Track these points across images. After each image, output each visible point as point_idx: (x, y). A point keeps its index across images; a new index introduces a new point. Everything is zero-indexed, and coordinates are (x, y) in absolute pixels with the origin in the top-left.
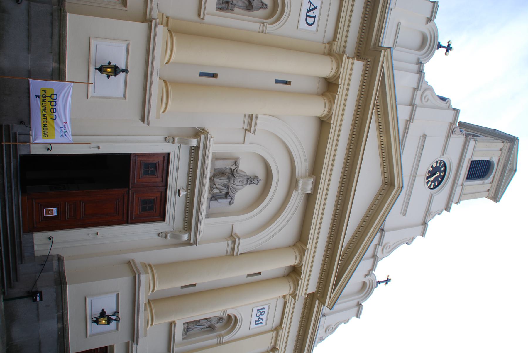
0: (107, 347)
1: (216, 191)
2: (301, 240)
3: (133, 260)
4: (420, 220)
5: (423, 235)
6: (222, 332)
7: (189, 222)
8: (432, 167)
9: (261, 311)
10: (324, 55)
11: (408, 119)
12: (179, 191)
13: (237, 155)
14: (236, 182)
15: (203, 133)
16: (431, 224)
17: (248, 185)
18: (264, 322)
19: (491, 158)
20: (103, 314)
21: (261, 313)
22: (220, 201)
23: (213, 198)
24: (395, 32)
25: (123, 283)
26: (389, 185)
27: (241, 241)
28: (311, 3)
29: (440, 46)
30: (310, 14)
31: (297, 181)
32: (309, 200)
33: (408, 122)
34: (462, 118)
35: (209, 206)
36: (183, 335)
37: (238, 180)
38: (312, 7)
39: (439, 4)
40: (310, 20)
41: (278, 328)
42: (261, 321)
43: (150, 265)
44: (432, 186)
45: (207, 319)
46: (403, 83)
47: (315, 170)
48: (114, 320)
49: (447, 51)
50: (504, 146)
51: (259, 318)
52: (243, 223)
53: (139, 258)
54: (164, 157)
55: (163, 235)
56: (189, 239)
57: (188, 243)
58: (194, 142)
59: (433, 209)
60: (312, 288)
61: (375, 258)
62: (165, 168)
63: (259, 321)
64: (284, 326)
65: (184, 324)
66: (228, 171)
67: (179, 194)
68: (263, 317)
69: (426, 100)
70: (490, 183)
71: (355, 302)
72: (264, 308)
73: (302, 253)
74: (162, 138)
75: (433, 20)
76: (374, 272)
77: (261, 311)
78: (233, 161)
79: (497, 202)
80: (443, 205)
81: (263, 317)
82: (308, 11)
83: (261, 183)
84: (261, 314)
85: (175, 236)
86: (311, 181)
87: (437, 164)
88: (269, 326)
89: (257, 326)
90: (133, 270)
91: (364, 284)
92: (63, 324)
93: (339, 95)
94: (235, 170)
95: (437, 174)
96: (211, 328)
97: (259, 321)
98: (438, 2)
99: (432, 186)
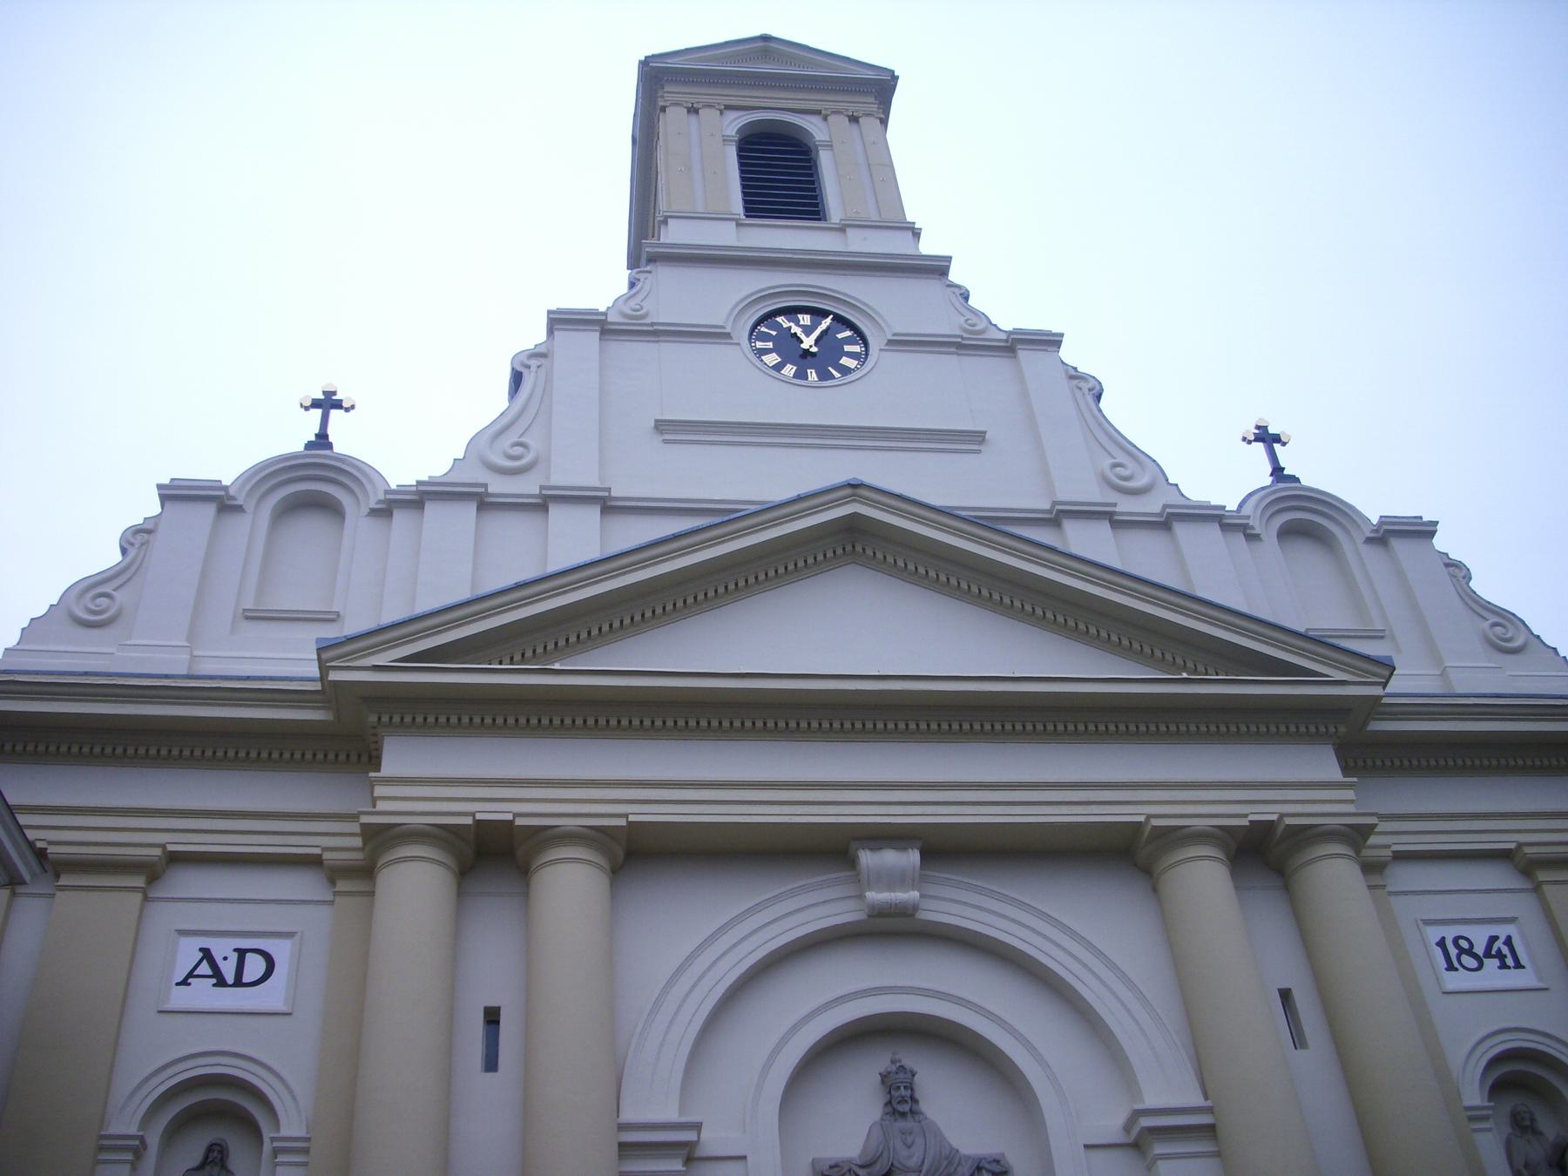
2: (1126, 853)
4: (996, 366)
5: (1051, 342)
8: (778, 367)
9: (1453, 952)
10: (372, 894)
11: (597, 510)
14: (913, 1162)
16: (1007, 316)
17: (924, 1106)
18: (1502, 931)
19: (726, 140)
21: (1462, 951)
24: (273, 625)
26: (855, 540)
27: (1151, 1101)
28: (191, 975)
29: (322, 440)
30: (229, 973)
31: (880, 912)
32: (947, 849)
33: (609, 506)
34: (603, 282)
37: (903, 1152)
38: (205, 968)
39: (167, 481)
40: (255, 967)
42: (1498, 944)
44: (856, 349)
46: (450, 568)
49: (338, 405)
50: (676, 104)
51: (1488, 954)
59: (944, 324)
60: (1322, 765)
61: (1180, 516)
63: (1503, 954)
64: (1507, 842)
68: (1479, 937)
69: (518, 450)
70: (825, 119)
71: (1372, 555)
72: (1441, 943)
73: (1172, 838)
75: (226, 488)
76: (1232, 506)
77: (1453, 952)
79: (895, 79)
80: (924, 288)
81: (1479, 937)
82: (221, 982)
84: (1470, 952)
86: (867, 859)
87: (767, 351)
88: (1522, 906)
89: (1523, 960)
91: (1288, 533)
95: (812, 336)
97: (1500, 956)
98: (159, 487)
99: (856, 349)
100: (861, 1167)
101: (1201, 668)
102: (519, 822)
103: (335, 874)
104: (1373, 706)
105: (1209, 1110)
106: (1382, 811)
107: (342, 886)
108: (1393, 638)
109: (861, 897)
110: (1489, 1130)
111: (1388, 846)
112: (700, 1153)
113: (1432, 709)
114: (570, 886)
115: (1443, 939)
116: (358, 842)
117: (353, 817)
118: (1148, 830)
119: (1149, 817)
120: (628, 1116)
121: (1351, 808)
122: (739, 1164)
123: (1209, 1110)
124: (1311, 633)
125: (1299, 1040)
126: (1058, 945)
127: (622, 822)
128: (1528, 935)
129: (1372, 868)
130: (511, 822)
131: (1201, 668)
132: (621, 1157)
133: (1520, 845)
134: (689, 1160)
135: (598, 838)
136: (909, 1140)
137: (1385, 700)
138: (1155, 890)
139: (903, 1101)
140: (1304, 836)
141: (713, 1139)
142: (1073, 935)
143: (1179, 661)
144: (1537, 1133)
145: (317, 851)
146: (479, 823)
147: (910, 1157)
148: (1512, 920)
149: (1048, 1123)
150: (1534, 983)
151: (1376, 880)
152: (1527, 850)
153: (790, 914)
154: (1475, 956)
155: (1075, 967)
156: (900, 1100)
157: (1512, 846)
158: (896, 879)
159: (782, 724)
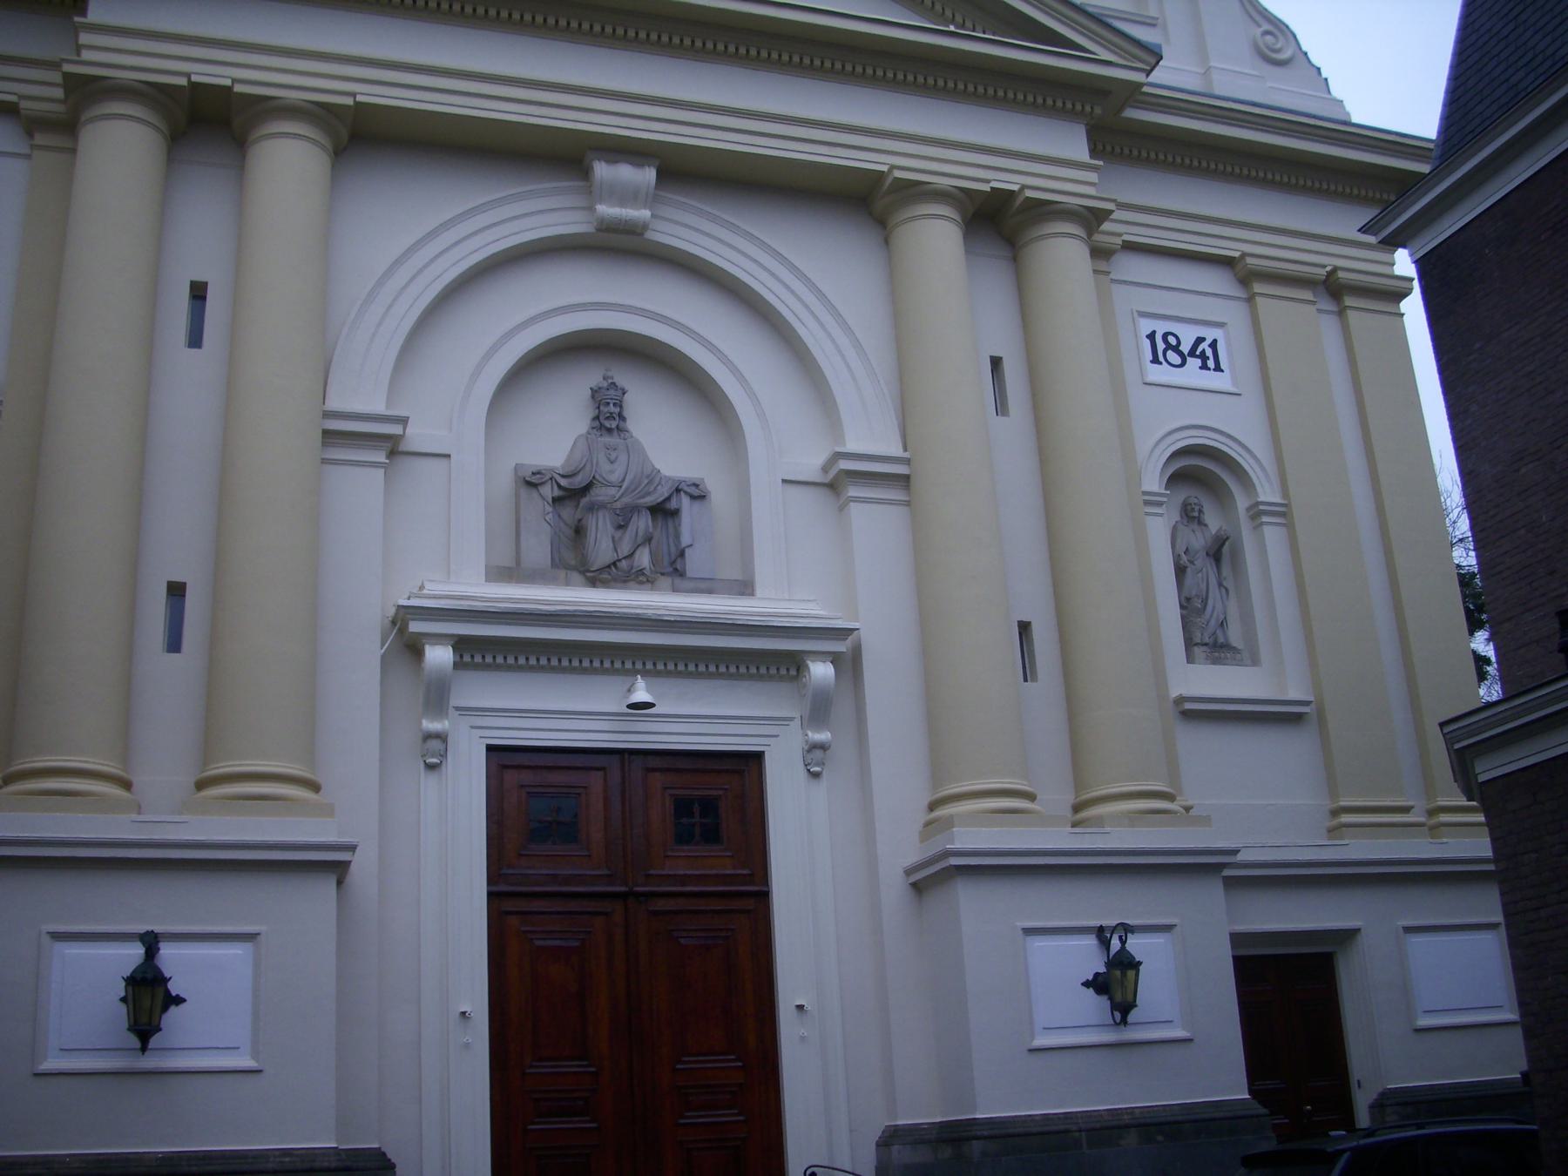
0: (1236, 959)
1: (644, 559)
2: (862, 201)
3: (909, 872)
6: (1242, 503)
7: (767, 659)
9: (1161, 346)
10: (74, 151)
12: (631, 706)
13: (505, 482)
15: (403, 630)
17: (631, 425)
18: (1210, 334)
20: (1098, 984)
21: (1168, 346)
22: (685, 540)
23: (673, 569)
25: (979, 911)
27: (852, 446)
32: (683, 171)
35: (708, 586)
36: (1240, 663)
37: (605, 467)
41: (1246, 275)
43: (932, 806)
45: (1180, 571)
47: (565, 157)
48: (1123, 942)
51: (1192, 353)
52: (783, 439)
53: (902, 848)
54: (506, 767)
55: (816, 759)
56: (835, 659)
57: (850, 664)
58: (439, 656)
60: (1072, 143)
62: (549, 760)
65: (1190, 659)
66: (568, 512)
67: (649, 705)
72: (1152, 336)
73: (912, 192)
74: (429, 783)
77: (1161, 346)
78: (524, 491)
83: (625, 377)
85: (820, 709)
86: (602, 171)
88: (1234, 314)
90: (935, 878)
92: (1127, 1126)
93: (234, 81)
94: (563, 482)
96: (1220, 551)
100: (563, 476)
101: (969, 24)
102: (238, 88)
103: (33, 125)
104: (1132, 93)
105: (907, 462)
106: (1121, 199)
107: (40, 139)
108: (1165, 29)
109: (591, 209)
110: (1161, 515)
111: (1120, 235)
112: (403, 447)
113: (1182, 105)
114: (288, 163)
115: (1154, 332)
116: (59, 93)
117: (54, 65)
118: (889, 181)
119: (893, 167)
120: (334, 404)
121: (1091, 191)
122: (444, 461)
123: (907, 462)
124: (1090, 10)
125: (1001, 407)
126: (787, 287)
127: (349, 101)
128: (1233, 343)
129: (1100, 253)
130: (229, 89)
131: (969, 24)
132: (324, 444)
133: (1244, 255)
134: (393, 453)
135: (323, 116)
136: (613, 457)
137: (1145, 89)
138: (887, 242)
139: (611, 417)
140: (1042, 211)
141: (419, 435)
142: (794, 269)
143: (948, 13)
144: (1201, 523)
145: (13, 98)
146: (195, 86)
147: (612, 472)
148: (1221, 325)
149: (751, 455)
150: (1229, 388)
151: (1103, 266)
152: (1249, 260)
153: (516, 218)
154: (1181, 354)
155: (798, 307)
156: (608, 417)
157: (1237, 254)
158: (627, 196)
159: (516, 16)
